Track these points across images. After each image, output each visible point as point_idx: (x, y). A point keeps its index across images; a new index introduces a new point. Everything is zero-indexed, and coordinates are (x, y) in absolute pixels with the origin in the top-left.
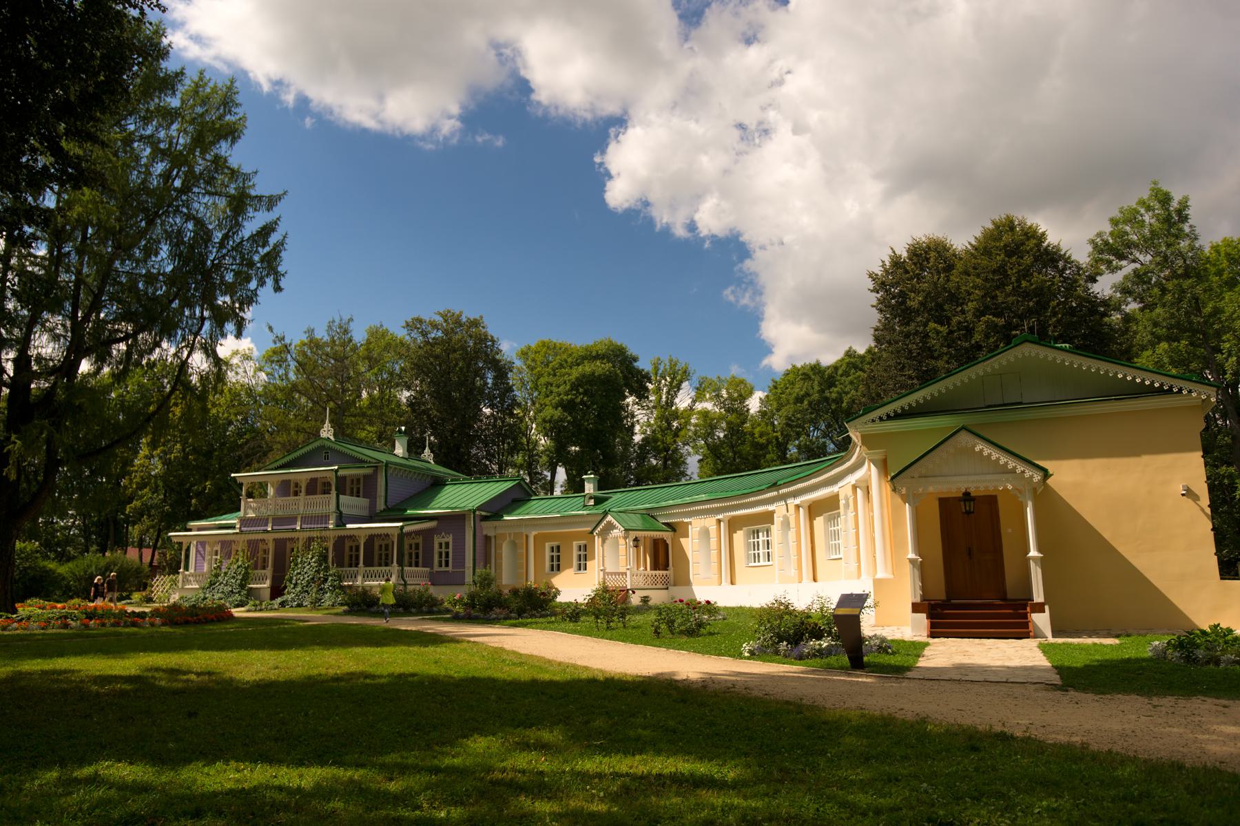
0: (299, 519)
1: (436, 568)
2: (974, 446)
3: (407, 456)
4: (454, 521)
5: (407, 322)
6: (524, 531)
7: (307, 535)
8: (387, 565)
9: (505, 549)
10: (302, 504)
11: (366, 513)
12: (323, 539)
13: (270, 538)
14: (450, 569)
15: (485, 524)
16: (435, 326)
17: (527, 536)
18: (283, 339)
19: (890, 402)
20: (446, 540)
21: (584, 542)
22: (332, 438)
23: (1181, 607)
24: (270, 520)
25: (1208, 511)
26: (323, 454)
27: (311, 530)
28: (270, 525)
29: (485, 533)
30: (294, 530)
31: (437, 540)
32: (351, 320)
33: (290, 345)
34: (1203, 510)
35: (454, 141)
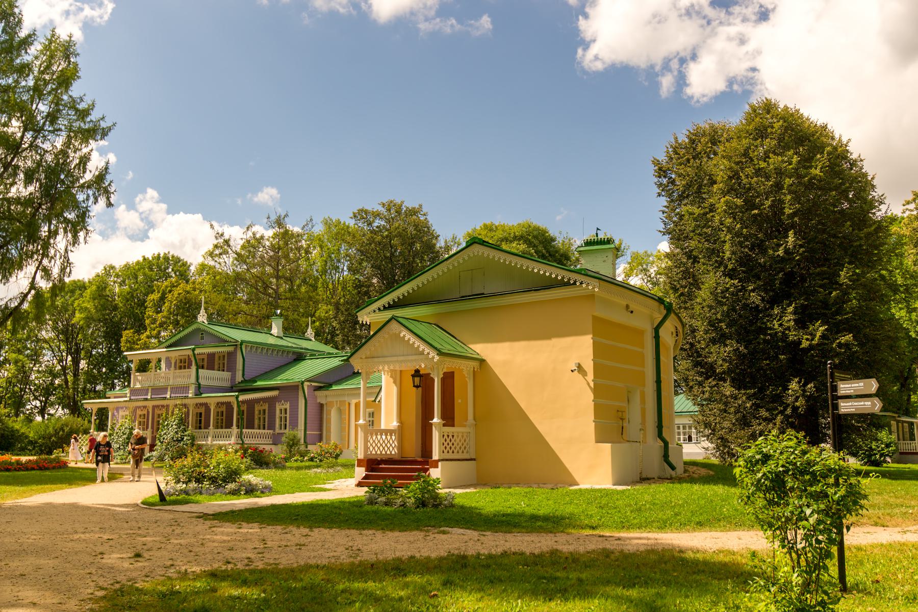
0: (169, 389)
1: (277, 431)
2: (400, 333)
3: (282, 335)
4: (291, 390)
5: (354, 213)
8: (206, 428)
11: (227, 384)
15: (318, 393)
16: (377, 215)
17: (349, 404)
18: (222, 235)
19: (376, 300)
20: (284, 407)
23: (568, 466)
24: (150, 391)
25: (592, 384)
27: (137, 400)
28: (150, 394)
29: (318, 401)
31: (278, 407)
32: (286, 215)
33: (229, 240)
34: (588, 384)
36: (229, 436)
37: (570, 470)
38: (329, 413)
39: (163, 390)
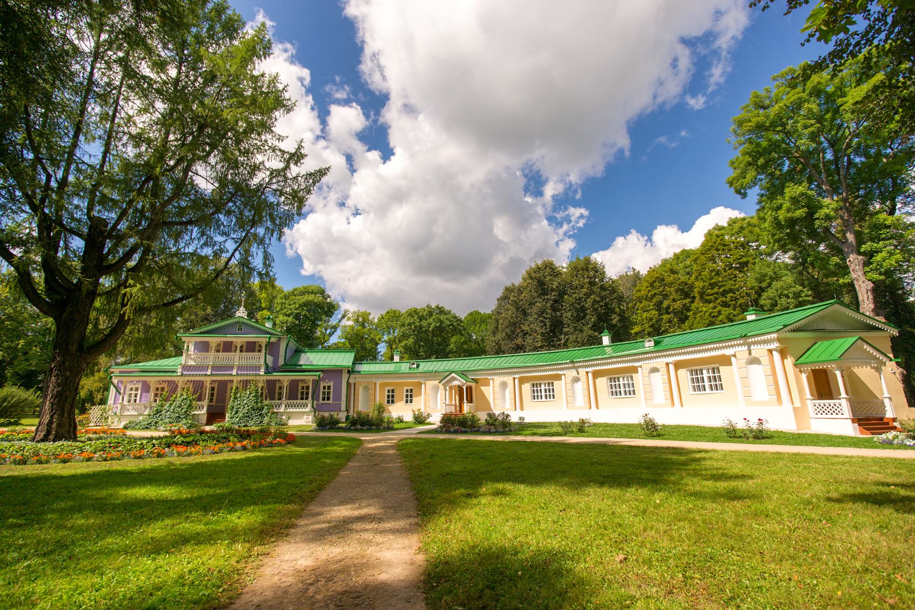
1: (321, 401)
6: (374, 380)
7: (240, 378)
9: (361, 392)
10: (236, 358)
12: (257, 382)
13: (209, 379)
14: (331, 401)
21: (393, 388)
22: (246, 317)
26: (240, 327)
30: (259, 375)
31: (322, 385)
35: (688, 107)
36: (305, 406)
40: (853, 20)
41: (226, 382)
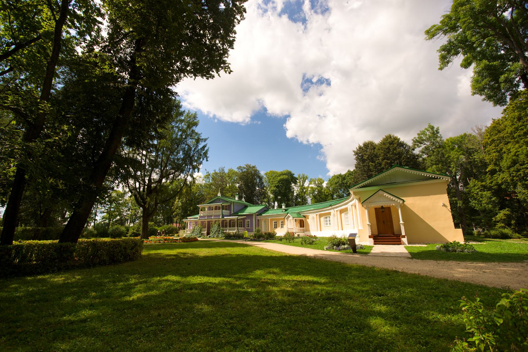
4: (250, 216)
6: (268, 218)
9: (263, 223)
12: (219, 221)
13: (206, 220)
15: (258, 216)
16: (244, 168)
25: (450, 210)
36: (235, 230)
37: (446, 238)
38: (261, 222)
39: (211, 216)
40: (108, 36)
41: (210, 221)
